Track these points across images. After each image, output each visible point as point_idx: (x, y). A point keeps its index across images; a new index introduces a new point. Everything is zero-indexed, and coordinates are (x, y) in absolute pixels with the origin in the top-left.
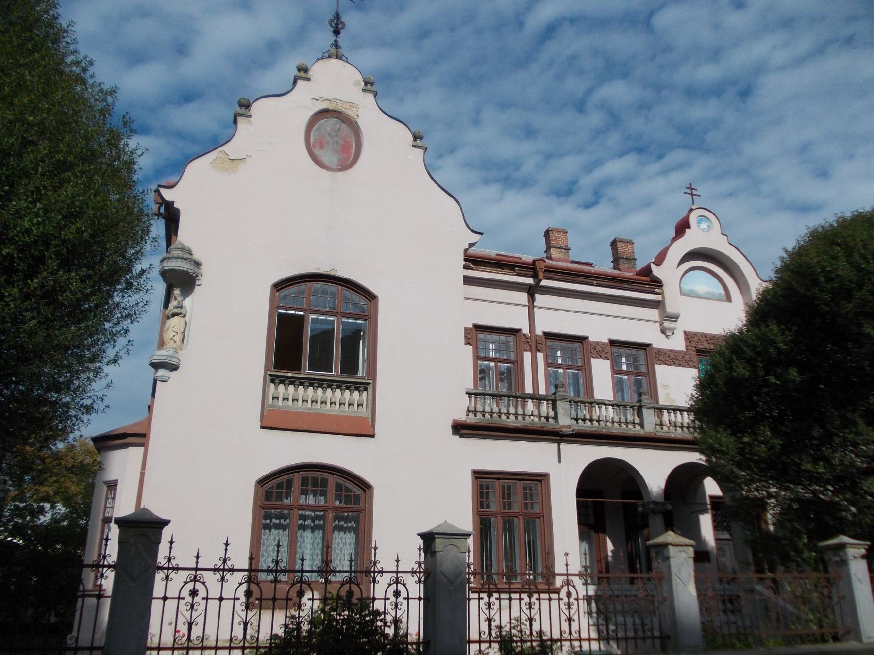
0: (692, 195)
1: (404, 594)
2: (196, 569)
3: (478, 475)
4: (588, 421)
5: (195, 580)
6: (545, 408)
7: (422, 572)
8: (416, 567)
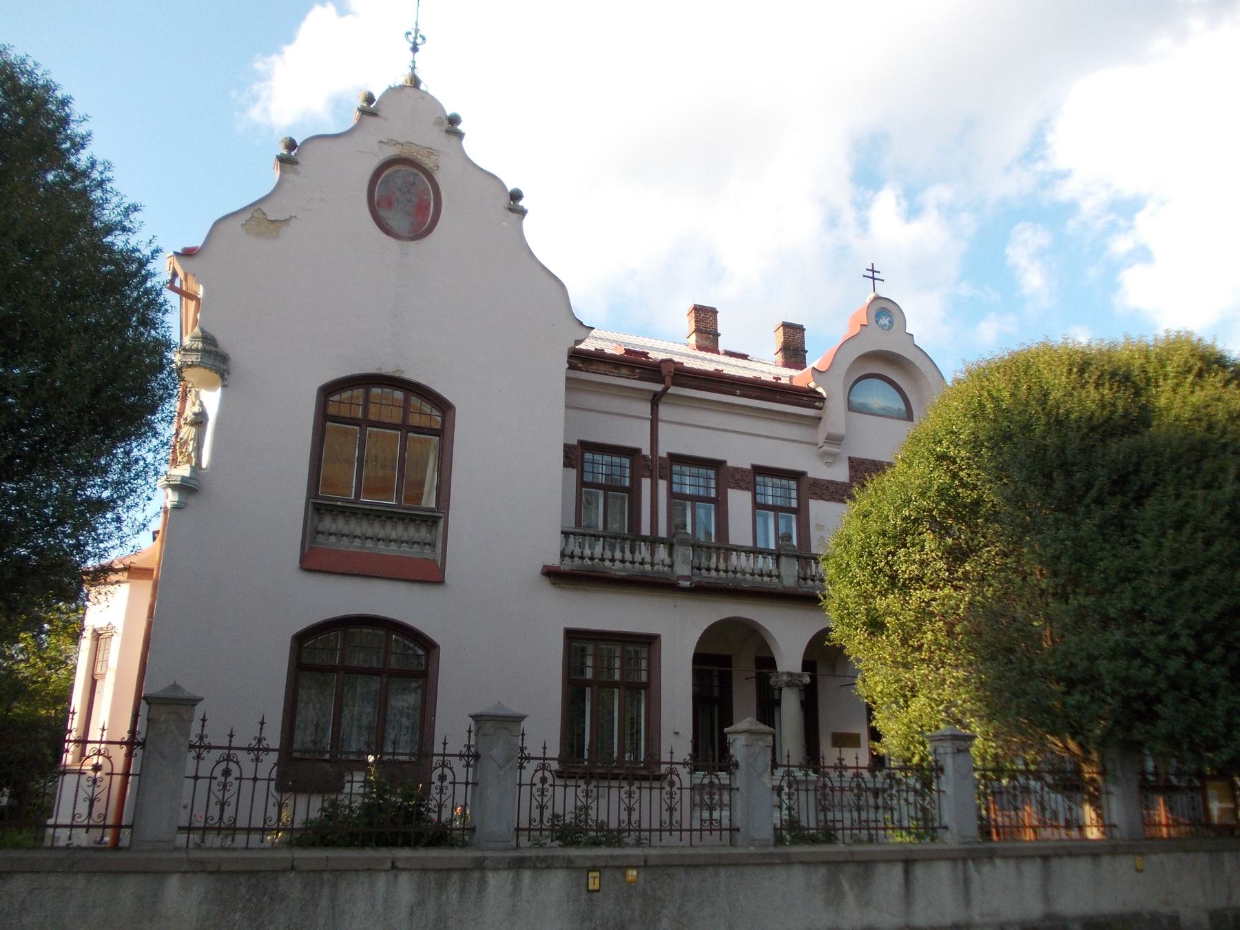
0: (874, 279)
1: (450, 778)
2: (230, 748)
3: (572, 635)
4: (713, 571)
5: (228, 759)
6: (662, 552)
7: (471, 756)
8: (464, 750)
